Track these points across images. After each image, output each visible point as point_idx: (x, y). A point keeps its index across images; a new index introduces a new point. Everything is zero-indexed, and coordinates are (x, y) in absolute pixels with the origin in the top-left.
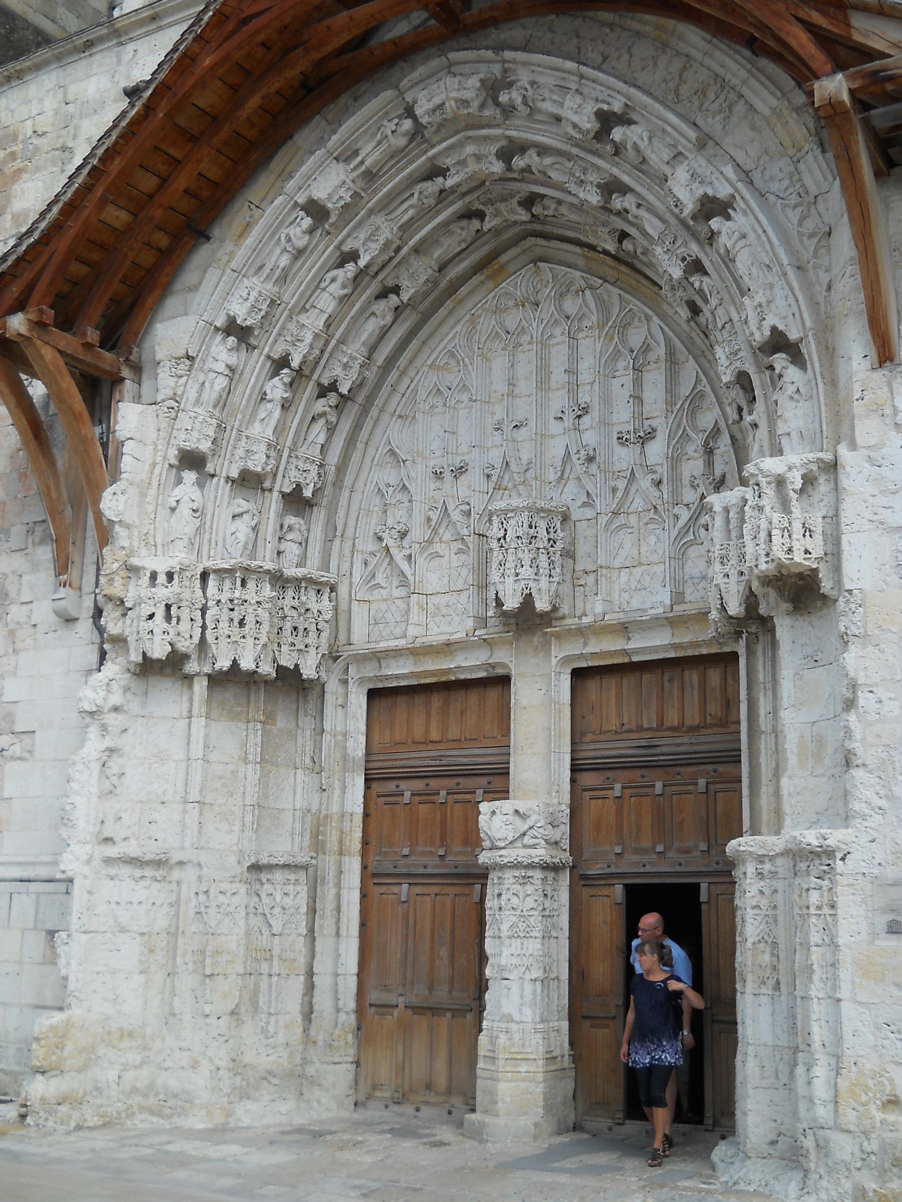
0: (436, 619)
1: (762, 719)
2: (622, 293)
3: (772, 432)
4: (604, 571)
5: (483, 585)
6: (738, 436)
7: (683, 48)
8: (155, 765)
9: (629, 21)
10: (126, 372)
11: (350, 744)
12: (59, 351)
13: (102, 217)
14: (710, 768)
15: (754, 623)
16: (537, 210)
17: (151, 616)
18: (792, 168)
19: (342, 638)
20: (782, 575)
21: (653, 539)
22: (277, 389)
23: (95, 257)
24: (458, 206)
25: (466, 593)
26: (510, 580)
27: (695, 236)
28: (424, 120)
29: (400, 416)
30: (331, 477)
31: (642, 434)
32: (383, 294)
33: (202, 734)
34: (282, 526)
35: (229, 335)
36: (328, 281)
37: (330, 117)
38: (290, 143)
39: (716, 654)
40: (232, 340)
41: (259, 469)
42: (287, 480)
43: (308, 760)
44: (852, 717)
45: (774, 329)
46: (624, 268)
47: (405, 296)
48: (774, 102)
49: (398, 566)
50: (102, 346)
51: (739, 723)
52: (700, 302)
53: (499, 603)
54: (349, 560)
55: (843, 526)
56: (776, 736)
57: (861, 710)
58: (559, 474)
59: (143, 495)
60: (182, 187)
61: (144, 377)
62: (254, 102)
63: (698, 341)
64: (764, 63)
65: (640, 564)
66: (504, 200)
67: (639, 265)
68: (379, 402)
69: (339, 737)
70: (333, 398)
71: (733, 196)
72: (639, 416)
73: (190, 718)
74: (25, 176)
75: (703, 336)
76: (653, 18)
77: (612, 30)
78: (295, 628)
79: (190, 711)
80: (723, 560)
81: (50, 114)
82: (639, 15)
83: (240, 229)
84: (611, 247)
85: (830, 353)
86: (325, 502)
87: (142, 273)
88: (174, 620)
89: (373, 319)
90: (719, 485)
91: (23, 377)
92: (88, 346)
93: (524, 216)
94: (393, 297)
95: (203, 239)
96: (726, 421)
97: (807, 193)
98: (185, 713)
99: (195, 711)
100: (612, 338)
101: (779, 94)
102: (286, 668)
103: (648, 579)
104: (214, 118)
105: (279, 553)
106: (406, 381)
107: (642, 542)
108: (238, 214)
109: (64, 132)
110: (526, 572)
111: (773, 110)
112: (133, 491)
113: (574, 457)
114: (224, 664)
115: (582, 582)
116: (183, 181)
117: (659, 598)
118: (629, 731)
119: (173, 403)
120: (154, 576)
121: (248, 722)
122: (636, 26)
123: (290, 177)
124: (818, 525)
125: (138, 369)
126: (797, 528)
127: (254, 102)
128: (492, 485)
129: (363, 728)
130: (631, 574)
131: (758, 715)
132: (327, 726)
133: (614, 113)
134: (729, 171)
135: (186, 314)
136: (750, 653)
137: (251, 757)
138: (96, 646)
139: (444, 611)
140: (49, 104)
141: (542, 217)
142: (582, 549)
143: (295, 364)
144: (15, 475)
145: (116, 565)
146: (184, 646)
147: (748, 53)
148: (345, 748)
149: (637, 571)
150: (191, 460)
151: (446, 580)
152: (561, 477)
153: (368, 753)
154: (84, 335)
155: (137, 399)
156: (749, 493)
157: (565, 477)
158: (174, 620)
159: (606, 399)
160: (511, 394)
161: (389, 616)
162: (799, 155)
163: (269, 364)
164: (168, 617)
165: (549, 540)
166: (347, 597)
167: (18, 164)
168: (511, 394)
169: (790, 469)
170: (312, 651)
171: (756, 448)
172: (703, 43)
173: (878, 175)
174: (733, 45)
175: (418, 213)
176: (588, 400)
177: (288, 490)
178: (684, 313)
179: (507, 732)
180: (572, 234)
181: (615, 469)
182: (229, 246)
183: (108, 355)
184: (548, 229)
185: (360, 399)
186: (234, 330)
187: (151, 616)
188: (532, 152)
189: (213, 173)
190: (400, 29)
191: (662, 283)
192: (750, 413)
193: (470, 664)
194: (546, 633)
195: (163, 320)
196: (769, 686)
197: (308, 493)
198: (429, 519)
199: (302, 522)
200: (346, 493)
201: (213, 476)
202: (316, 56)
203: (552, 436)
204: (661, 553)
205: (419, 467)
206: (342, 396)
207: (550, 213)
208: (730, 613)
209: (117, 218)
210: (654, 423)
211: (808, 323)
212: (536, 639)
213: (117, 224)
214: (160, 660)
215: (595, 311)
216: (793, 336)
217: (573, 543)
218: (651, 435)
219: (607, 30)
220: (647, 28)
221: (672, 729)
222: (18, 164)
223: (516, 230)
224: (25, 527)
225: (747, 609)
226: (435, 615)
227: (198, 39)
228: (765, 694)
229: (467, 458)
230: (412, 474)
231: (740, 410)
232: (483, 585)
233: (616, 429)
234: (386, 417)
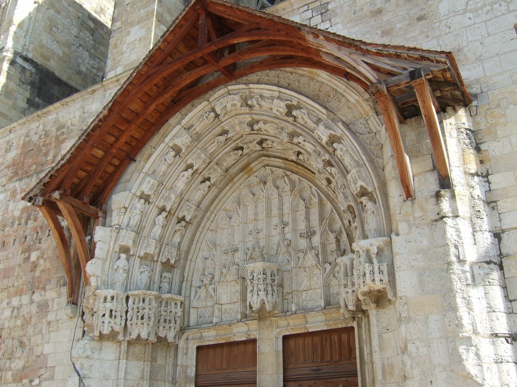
0: (225, 315)
1: (366, 357)
2: (300, 177)
3: (363, 230)
4: (296, 292)
5: (244, 299)
6: (350, 233)
7: (320, 79)
8: (104, 381)
9: (298, 71)
10: (100, 214)
11: (189, 371)
12: (72, 206)
13: (92, 153)
14: (345, 379)
15: (360, 312)
16: (264, 145)
17: (104, 315)
18: (366, 123)
19: (186, 324)
20: (371, 290)
21: (316, 278)
22: (161, 218)
23: (89, 168)
24: (233, 145)
25: (238, 303)
26: (255, 296)
27: (328, 152)
28: (219, 113)
29: (211, 230)
30: (183, 256)
31: (310, 234)
32: (203, 182)
33: (124, 368)
34: (161, 277)
35: (141, 198)
36: (181, 176)
37: (183, 113)
38: (167, 123)
39: (345, 328)
40: (142, 201)
41: (152, 252)
42: (164, 257)
43: (170, 378)
44: (406, 358)
45: (362, 187)
46: (300, 167)
47: (213, 181)
48: (357, 98)
49: (209, 292)
50: (91, 204)
51: (355, 358)
52: (331, 178)
53: (251, 307)
54: (189, 290)
55: (395, 268)
56: (372, 364)
57: (409, 352)
58: (276, 251)
59: (104, 264)
60: (124, 141)
61: (108, 216)
62: (153, 107)
63: (331, 195)
64: (352, 83)
65: (311, 289)
66: (251, 142)
67: (306, 165)
68: (202, 225)
69: (184, 368)
70: (183, 223)
71: (342, 134)
72: (309, 227)
73: (119, 359)
74: (67, 141)
75: (333, 193)
76: (308, 69)
77: (291, 74)
78: (165, 320)
79: (120, 357)
80: (345, 286)
81: (78, 118)
82: (301, 68)
83: (147, 157)
84: (294, 158)
85: (385, 195)
86: (180, 266)
87: (108, 175)
88: (113, 317)
89: (199, 191)
90: (344, 253)
91: (58, 216)
92: (85, 204)
93: (258, 148)
94: (207, 182)
95: (133, 161)
96: (344, 227)
97: (372, 132)
98: (117, 358)
99: (121, 357)
100: (296, 195)
101: (358, 94)
102: (161, 337)
103: (314, 296)
104: (137, 114)
105: (160, 288)
106: (213, 215)
107: (311, 280)
108: (147, 150)
109: (82, 124)
110: (262, 293)
111: (356, 101)
112: (99, 262)
113: (282, 245)
114: (134, 336)
115: (286, 297)
116: (124, 139)
117: (319, 304)
118: (308, 363)
119: (118, 227)
120: (105, 299)
121: (144, 361)
122: (301, 72)
123: (167, 136)
124: (384, 268)
125: (105, 213)
126: (376, 270)
127: (153, 107)
128: (248, 257)
129: (194, 363)
130: (307, 293)
131: (364, 355)
132: (179, 363)
133: (293, 105)
134: (340, 125)
135: (125, 191)
136: (359, 326)
137: (145, 377)
138: (82, 329)
139: (229, 311)
140: (78, 114)
141: (266, 148)
142: (286, 283)
143: (168, 209)
144: (55, 258)
145: (91, 293)
146: (117, 328)
147: (345, 80)
148: (186, 372)
149: (310, 292)
150: (125, 250)
151: (229, 298)
152: (277, 253)
153: (197, 375)
154: (83, 199)
155: (104, 225)
156: (355, 256)
157: (279, 252)
158: (113, 317)
159: (295, 220)
160: (256, 220)
161: (206, 314)
162: (367, 117)
163: (157, 209)
164: (111, 316)
165: (272, 279)
166: (188, 306)
167: (65, 136)
168: (256, 220)
169: (372, 245)
170: (173, 329)
171: (357, 237)
172: (328, 77)
173: (401, 122)
174: (339, 77)
175: (217, 148)
176: (287, 220)
177: (164, 261)
178: (325, 182)
179: (255, 365)
180: (278, 154)
181: (299, 249)
182: (142, 163)
183: (92, 207)
184: (269, 153)
185: (195, 223)
186: (146, 198)
187: (104, 315)
188: (261, 122)
189: (137, 135)
190: (210, 79)
191: (315, 172)
192: (354, 222)
193: (239, 333)
194: (271, 320)
195: (116, 193)
196: (368, 341)
197: (172, 262)
198: (222, 273)
199: (170, 274)
200: (188, 262)
201: (133, 256)
202: (177, 89)
203: (273, 236)
204: (319, 284)
205: (218, 250)
206: (187, 222)
207: (270, 146)
208: (350, 309)
209: (98, 153)
210: (315, 229)
211: (376, 185)
212: (267, 323)
213: (99, 156)
214: (107, 335)
215: (288, 184)
216: (370, 189)
217: (282, 280)
218: (314, 233)
219: (290, 74)
220: (305, 73)
221: (327, 362)
222: (65, 136)
223: (256, 154)
224: (57, 279)
225: (357, 307)
226: (225, 313)
227: (131, 83)
228: (366, 345)
229: (238, 246)
230: (215, 254)
231: (350, 222)
232: (244, 299)
233: (299, 232)
234: (205, 230)
